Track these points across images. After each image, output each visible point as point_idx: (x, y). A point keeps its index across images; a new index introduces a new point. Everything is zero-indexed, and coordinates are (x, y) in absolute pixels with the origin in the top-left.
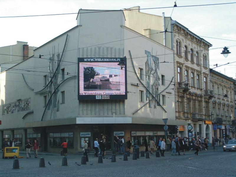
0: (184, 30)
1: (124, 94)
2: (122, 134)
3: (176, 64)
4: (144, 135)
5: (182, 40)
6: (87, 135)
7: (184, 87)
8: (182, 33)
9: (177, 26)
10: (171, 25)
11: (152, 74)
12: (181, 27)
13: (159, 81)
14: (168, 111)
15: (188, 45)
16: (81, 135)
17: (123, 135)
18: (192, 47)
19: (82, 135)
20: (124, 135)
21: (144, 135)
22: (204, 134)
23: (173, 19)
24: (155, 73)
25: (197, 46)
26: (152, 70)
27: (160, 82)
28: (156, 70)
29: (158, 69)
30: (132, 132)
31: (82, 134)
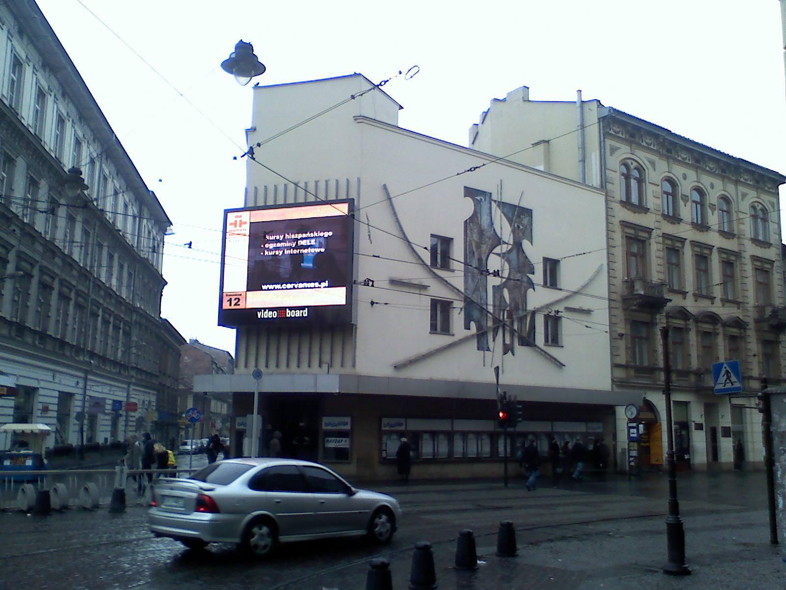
0: (656, 136)
1: (343, 302)
2: (345, 424)
3: (618, 228)
4: (549, 429)
5: (769, 205)
6: (339, 424)
7: (642, 293)
8: (769, 188)
9: (623, 124)
10: (599, 119)
11: (498, 255)
12: (705, 152)
13: (530, 276)
14: (585, 362)
15: (709, 188)
16: (382, 426)
17: (348, 427)
18: (723, 193)
19: (327, 425)
20: (351, 427)
21: (551, 430)
22: (663, 433)
23: (606, 103)
24: (510, 251)
25: (697, 172)
26: (499, 241)
27: (538, 277)
28: (518, 245)
29: (526, 244)
30: (385, 421)
31: (240, 422)
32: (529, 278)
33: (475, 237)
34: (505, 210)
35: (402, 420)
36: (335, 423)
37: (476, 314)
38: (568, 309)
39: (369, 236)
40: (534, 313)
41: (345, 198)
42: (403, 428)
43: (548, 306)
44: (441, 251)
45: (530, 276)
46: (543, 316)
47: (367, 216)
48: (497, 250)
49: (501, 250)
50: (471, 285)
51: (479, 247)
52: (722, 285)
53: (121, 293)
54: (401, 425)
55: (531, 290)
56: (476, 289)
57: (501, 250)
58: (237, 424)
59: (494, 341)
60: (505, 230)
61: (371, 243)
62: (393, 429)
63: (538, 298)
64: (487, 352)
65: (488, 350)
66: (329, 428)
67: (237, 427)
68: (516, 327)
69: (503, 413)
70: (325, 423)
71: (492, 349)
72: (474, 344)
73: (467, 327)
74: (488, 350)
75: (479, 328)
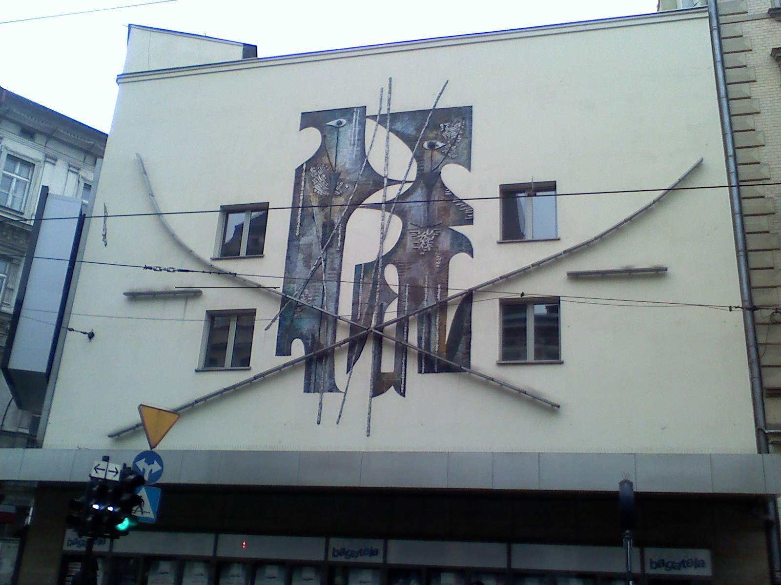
2: (699, 564)
6: (361, 552)
13: (461, 229)
31: (656, 559)
32: (452, 230)
33: (320, 188)
34: (399, 126)
35: (377, 544)
36: (673, 563)
37: (307, 325)
38: (576, 277)
39: (105, 236)
40: (468, 297)
41: (59, 194)
42: (378, 559)
43: (508, 279)
44: (245, 227)
45: (461, 229)
46: (498, 302)
47: (105, 207)
48: (377, 197)
49: (385, 196)
50: (301, 271)
51: (325, 204)
52: (432, 199)
53: (768, 316)
54: (374, 553)
55: (463, 256)
56: (314, 277)
57: (385, 196)
58: (66, 541)
59: (349, 369)
60: (394, 159)
61: (106, 245)
62: (352, 560)
63: (482, 262)
64: (327, 395)
65: (333, 388)
66: (662, 571)
67: (66, 548)
68: (413, 338)
69: (93, 519)
70: (652, 562)
71: (341, 387)
72: (299, 379)
73: (283, 349)
74: (333, 388)
75: (312, 344)
